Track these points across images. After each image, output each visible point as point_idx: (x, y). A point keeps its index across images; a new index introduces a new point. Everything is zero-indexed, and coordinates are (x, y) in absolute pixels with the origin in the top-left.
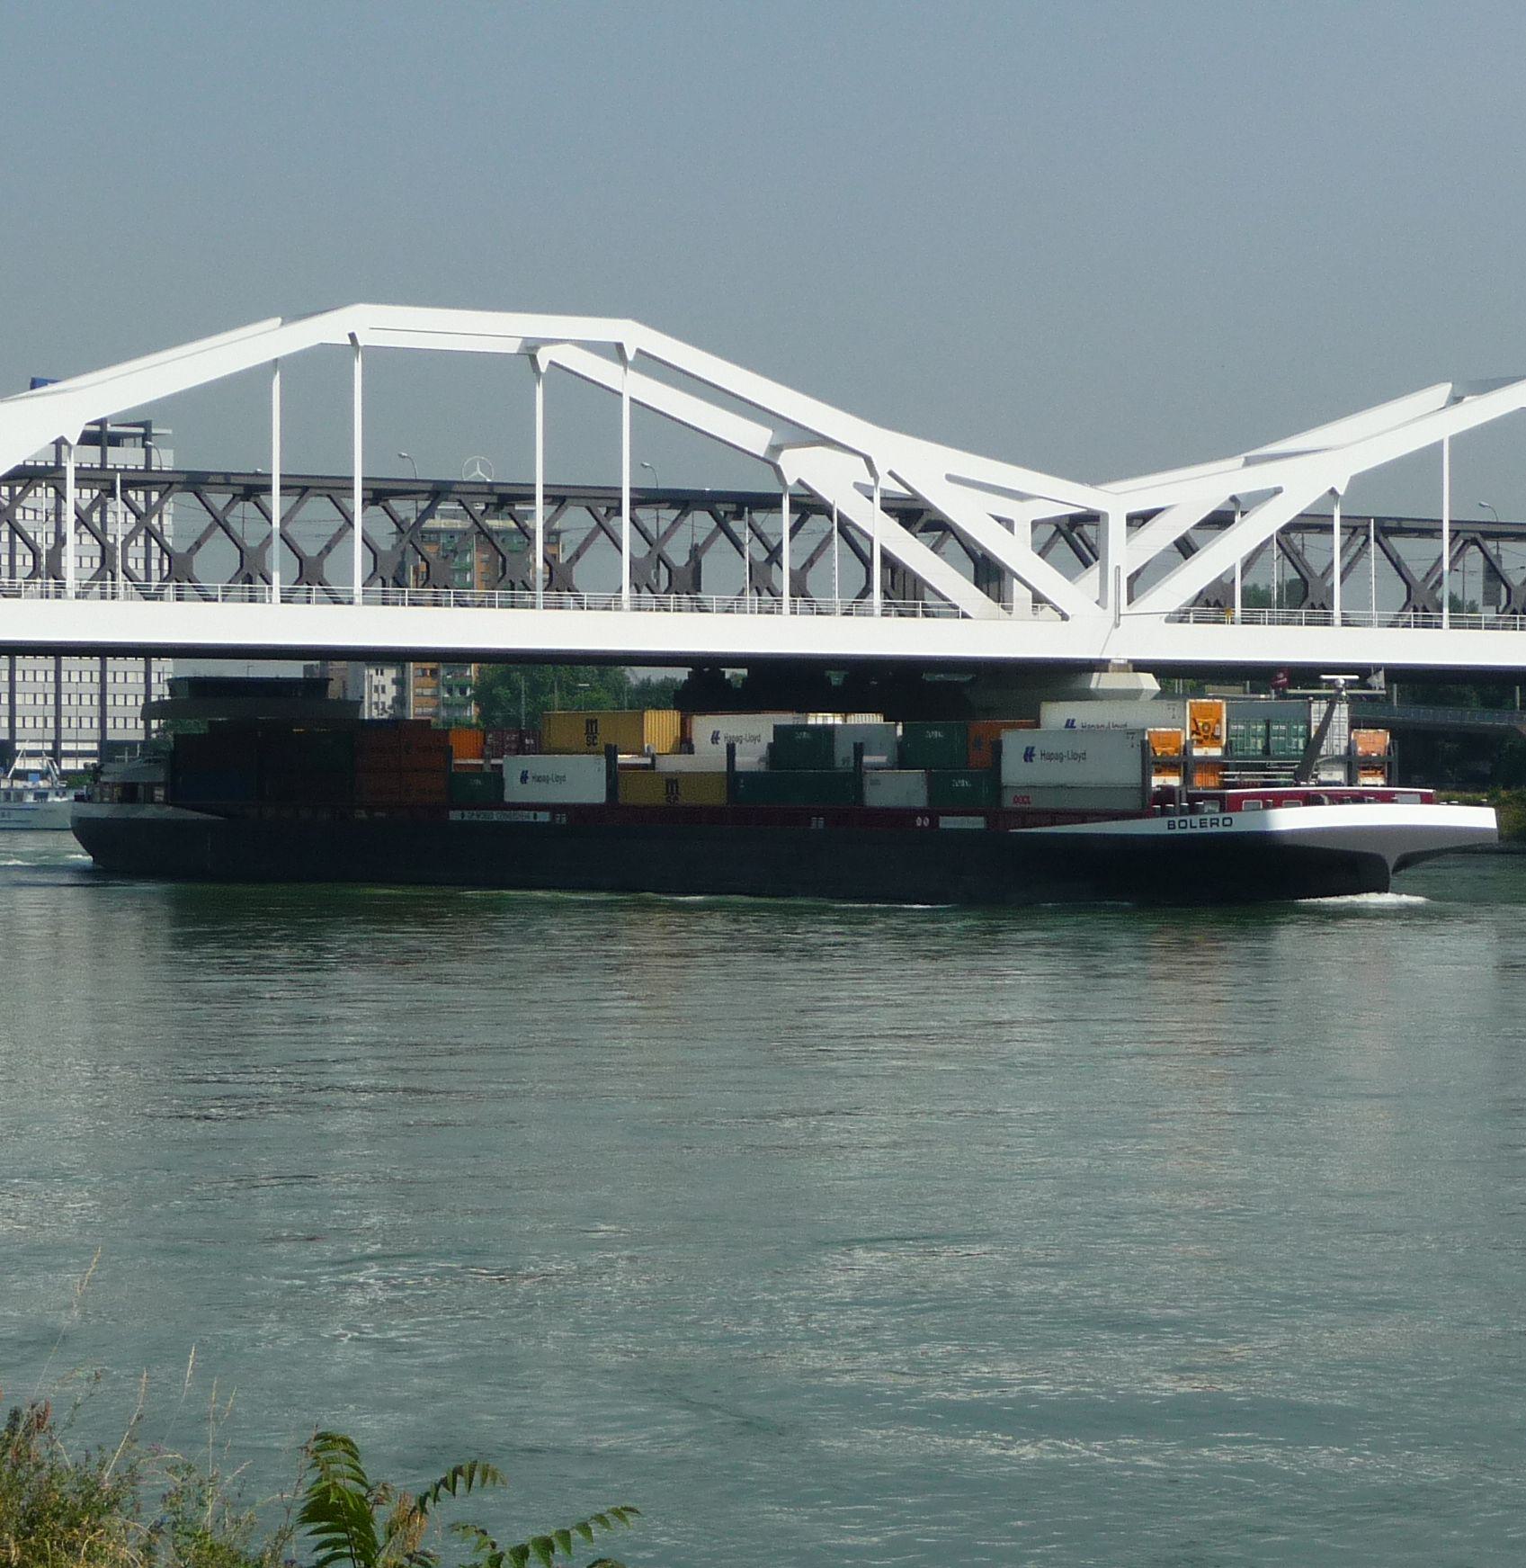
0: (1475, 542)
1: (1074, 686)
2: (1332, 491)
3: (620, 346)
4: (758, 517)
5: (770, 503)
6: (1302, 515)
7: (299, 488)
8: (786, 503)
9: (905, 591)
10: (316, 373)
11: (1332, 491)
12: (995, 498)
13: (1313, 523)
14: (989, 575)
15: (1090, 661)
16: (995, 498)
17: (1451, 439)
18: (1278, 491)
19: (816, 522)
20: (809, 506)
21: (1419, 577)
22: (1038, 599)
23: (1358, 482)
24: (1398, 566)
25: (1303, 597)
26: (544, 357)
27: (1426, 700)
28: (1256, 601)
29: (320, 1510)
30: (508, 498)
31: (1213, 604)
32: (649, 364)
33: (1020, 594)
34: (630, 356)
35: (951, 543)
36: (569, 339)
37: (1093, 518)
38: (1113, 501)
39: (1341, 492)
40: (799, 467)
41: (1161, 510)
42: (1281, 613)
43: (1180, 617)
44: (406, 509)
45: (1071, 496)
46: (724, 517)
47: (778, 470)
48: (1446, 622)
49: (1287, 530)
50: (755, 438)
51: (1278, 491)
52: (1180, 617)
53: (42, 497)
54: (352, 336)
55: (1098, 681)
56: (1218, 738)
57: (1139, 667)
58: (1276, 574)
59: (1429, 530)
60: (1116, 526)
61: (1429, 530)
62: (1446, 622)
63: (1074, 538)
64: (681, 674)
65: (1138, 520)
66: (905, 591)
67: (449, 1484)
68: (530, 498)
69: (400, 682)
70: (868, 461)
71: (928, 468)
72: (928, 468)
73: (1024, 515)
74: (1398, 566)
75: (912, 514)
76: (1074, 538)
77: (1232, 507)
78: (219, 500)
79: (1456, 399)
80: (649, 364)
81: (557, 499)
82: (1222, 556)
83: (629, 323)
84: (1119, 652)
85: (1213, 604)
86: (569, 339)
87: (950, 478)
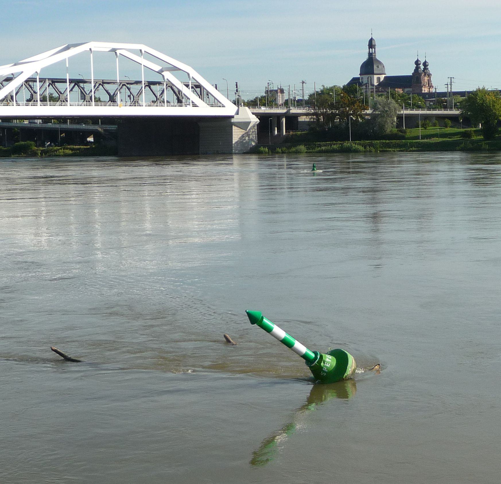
0: (125, 85)
2: (36, 72)
3: (141, 50)
6: (29, 78)
9: (180, 100)
11: (36, 72)
17: (69, 58)
18: (22, 72)
21: (112, 94)
23: (43, 70)
26: (118, 52)
27: (60, 122)
29: (378, 230)
34: (143, 52)
39: (39, 72)
47: (163, 76)
49: (26, 81)
51: (22, 72)
54: (90, 49)
59: (64, 81)
61: (64, 81)
62: (69, 105)
70: (189, 74)
77: (12, 76)
83: (92, 42)
86: (125, 48)
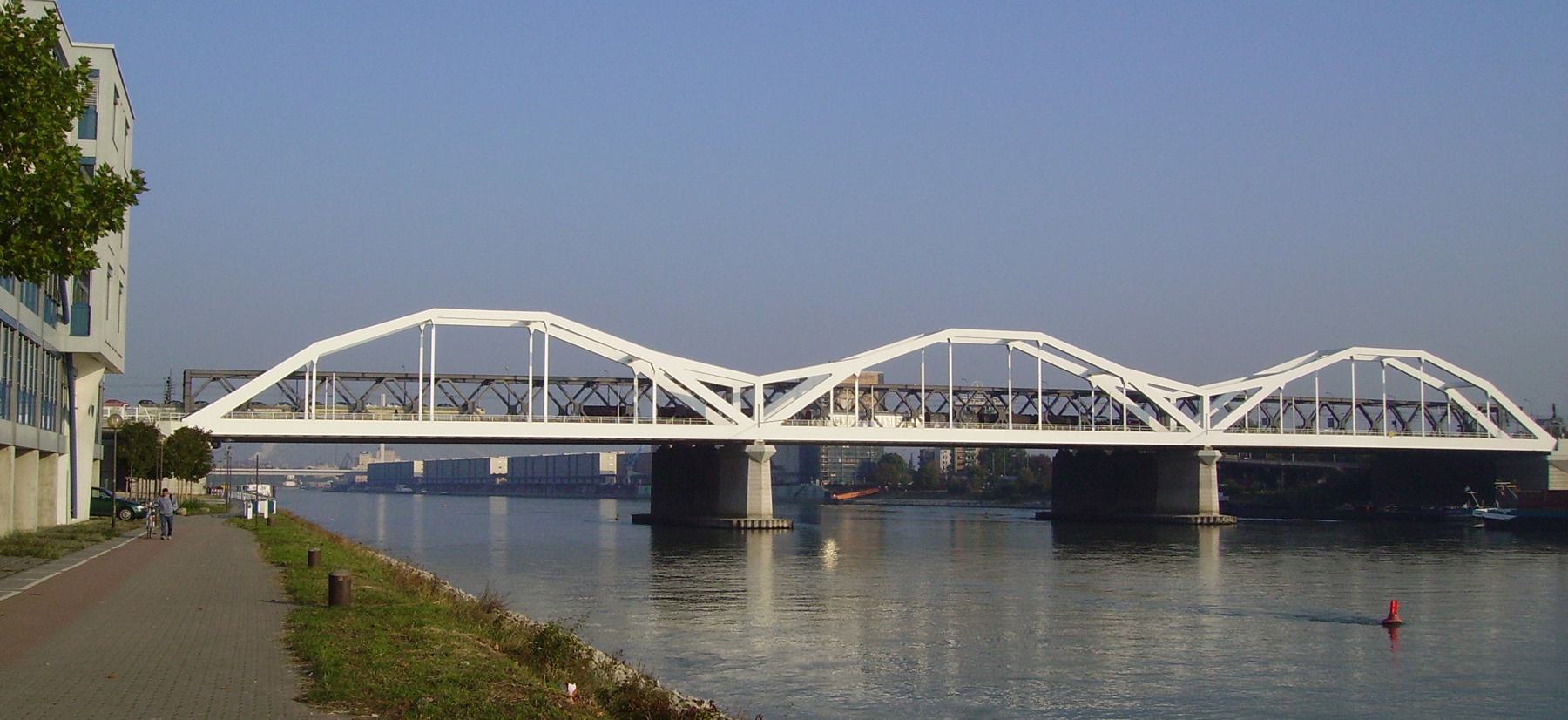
4: (1083, 399)
5: (1088, 393)
7: (1017, 392)
10: (938, 350)
12: (1164, 391)
13: (1272, 400)
14: (1162, 415)
16: (1164, 391)
19: (1103, 400)
20: (1100, 393)
22: (1179, 424)
24: (1366, 415)
25: (1270, 424)
28: (1253, 427)
30: (999, 393)
31: (1239, 427)
32: (1048, 348)
33: (1173, 423)
35: (1148, 407)
36: (1019, 339)
37: (1198, 398)
38: (1205, 392)
40: (1097, 381)
42: (574, 417)
43: (1227, 431)
44: (965, 398)
45: (1189, 390)
46: (1077, 401)
50: (1079, 370)
52: (1227, 431)
53: (847, 395)
55: (1200, 453)
56: (122, 486)
57: (1215, 448)
58: (1260, 416)
60: (1206, 402)
63: (1191, 405)
64: (647, 449)
65: (1213, 398)
66: (1467, 426)
69: (952, 455)
71: (1142, 381)
72: (1142, 381)
73: (1174, 396)
74: (1366, 415)
75: (1136, 396)
76: (1191, 405)
78: (904, 394)
79: (1319, 356)
80: (1048, 348)
81: (1017, 392)
82: (1241, 412)
84: (1208, 444)
85: (1239, 427)
86: (1019, 339)
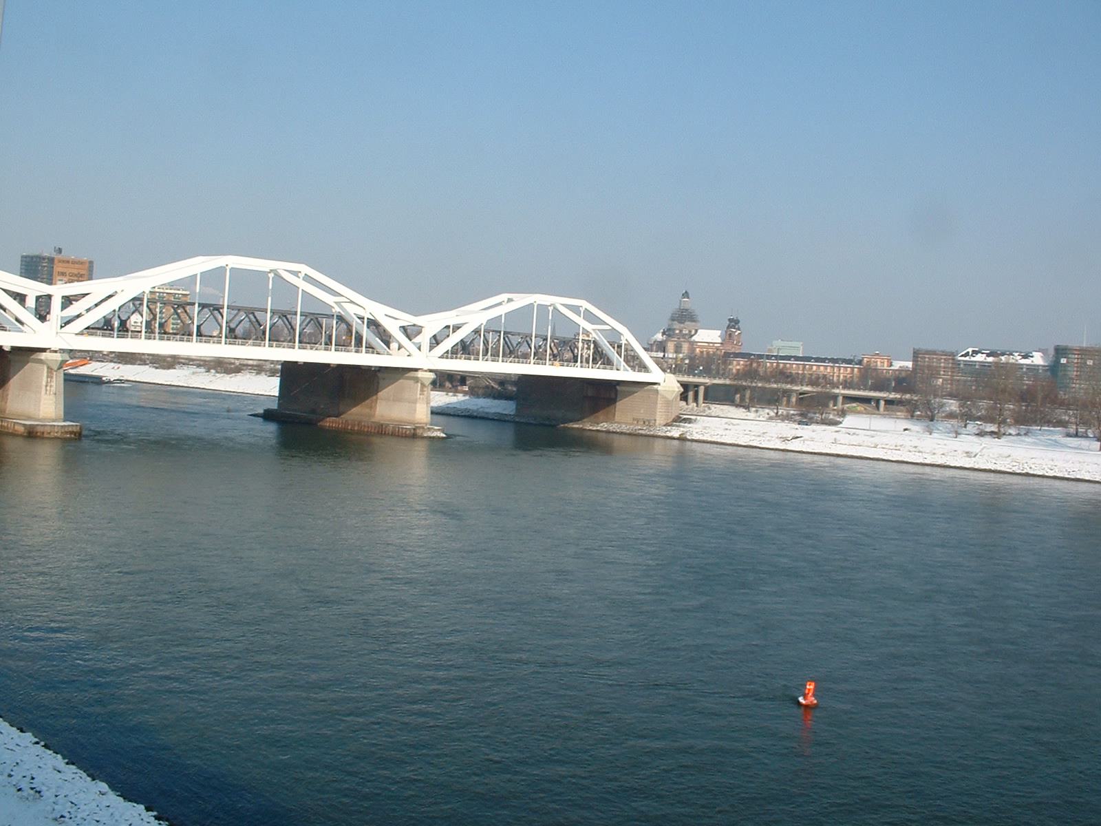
1: (32, 357)
8: (197, 305)
15: (34, 348)
17: (505, 314)
32: (308, 278)
33: (394, 346)
41: (88, 294)
43: (442, 357)
48: (115, 336)
57: (431, 371)
62: (115, 336)
63: (410, 332)
67: (844, 501)
68: (296, 314)
71: (379, 312)
72: (379, 312)
76: (410, 332)
80: (308, 278)
86: (281, 266)
87: (386, 315)
